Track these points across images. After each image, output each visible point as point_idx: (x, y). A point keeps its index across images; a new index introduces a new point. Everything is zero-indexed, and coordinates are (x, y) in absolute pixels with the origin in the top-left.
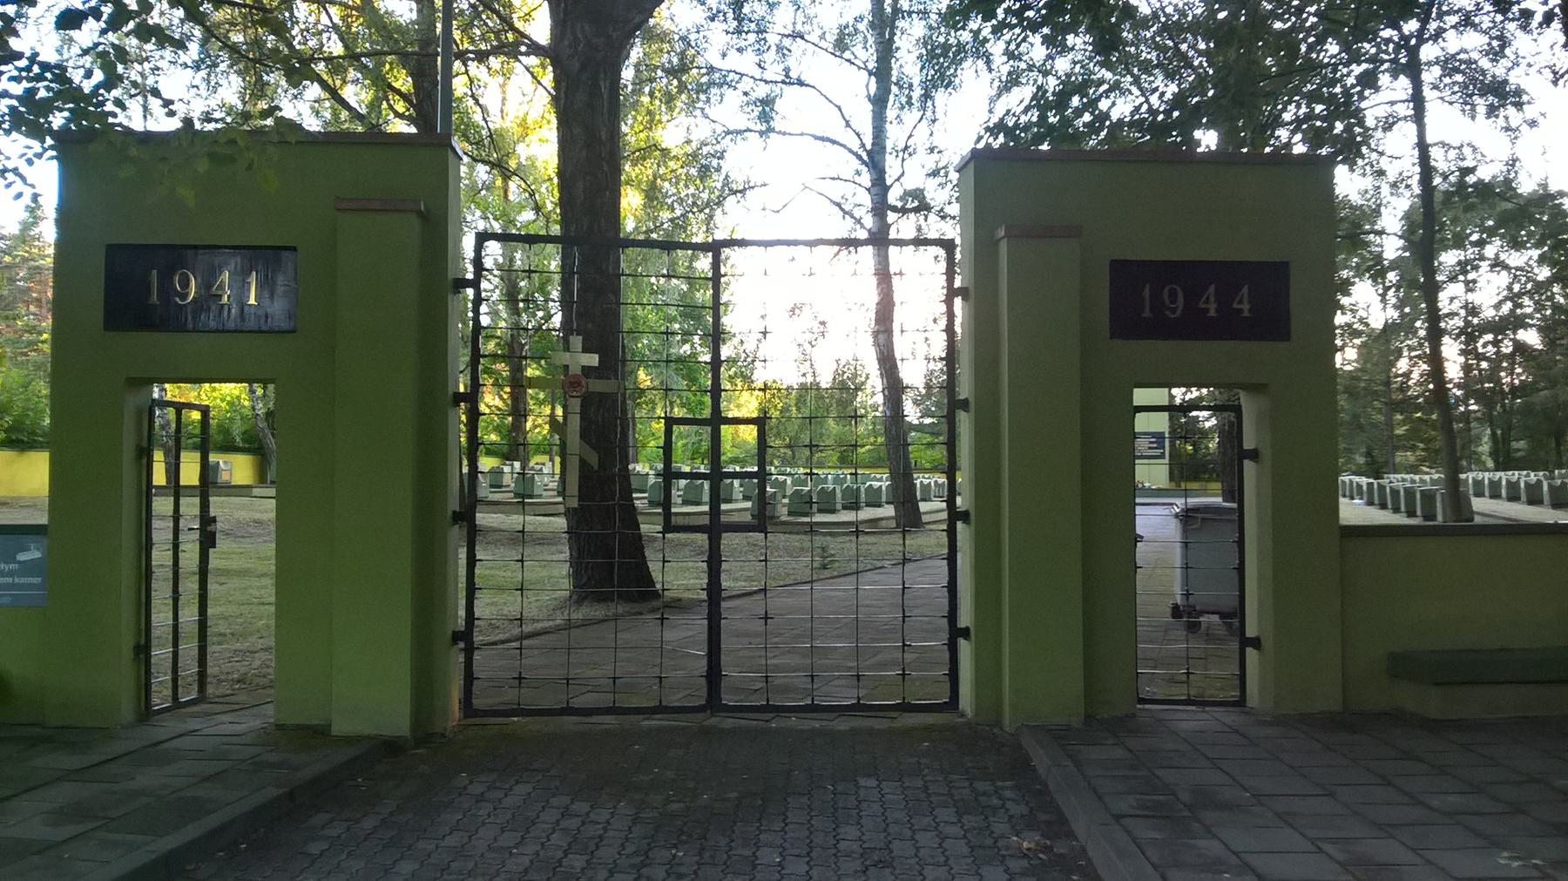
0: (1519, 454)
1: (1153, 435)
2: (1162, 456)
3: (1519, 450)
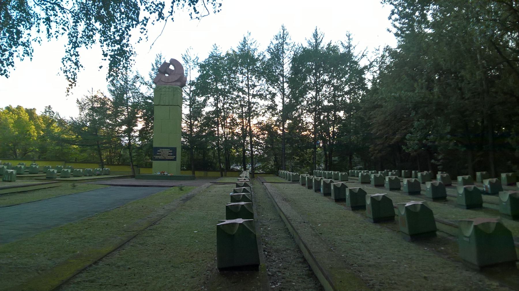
0: (335, 162)
1: (171, 149)
2: (175, 159)
3: (335, 161)
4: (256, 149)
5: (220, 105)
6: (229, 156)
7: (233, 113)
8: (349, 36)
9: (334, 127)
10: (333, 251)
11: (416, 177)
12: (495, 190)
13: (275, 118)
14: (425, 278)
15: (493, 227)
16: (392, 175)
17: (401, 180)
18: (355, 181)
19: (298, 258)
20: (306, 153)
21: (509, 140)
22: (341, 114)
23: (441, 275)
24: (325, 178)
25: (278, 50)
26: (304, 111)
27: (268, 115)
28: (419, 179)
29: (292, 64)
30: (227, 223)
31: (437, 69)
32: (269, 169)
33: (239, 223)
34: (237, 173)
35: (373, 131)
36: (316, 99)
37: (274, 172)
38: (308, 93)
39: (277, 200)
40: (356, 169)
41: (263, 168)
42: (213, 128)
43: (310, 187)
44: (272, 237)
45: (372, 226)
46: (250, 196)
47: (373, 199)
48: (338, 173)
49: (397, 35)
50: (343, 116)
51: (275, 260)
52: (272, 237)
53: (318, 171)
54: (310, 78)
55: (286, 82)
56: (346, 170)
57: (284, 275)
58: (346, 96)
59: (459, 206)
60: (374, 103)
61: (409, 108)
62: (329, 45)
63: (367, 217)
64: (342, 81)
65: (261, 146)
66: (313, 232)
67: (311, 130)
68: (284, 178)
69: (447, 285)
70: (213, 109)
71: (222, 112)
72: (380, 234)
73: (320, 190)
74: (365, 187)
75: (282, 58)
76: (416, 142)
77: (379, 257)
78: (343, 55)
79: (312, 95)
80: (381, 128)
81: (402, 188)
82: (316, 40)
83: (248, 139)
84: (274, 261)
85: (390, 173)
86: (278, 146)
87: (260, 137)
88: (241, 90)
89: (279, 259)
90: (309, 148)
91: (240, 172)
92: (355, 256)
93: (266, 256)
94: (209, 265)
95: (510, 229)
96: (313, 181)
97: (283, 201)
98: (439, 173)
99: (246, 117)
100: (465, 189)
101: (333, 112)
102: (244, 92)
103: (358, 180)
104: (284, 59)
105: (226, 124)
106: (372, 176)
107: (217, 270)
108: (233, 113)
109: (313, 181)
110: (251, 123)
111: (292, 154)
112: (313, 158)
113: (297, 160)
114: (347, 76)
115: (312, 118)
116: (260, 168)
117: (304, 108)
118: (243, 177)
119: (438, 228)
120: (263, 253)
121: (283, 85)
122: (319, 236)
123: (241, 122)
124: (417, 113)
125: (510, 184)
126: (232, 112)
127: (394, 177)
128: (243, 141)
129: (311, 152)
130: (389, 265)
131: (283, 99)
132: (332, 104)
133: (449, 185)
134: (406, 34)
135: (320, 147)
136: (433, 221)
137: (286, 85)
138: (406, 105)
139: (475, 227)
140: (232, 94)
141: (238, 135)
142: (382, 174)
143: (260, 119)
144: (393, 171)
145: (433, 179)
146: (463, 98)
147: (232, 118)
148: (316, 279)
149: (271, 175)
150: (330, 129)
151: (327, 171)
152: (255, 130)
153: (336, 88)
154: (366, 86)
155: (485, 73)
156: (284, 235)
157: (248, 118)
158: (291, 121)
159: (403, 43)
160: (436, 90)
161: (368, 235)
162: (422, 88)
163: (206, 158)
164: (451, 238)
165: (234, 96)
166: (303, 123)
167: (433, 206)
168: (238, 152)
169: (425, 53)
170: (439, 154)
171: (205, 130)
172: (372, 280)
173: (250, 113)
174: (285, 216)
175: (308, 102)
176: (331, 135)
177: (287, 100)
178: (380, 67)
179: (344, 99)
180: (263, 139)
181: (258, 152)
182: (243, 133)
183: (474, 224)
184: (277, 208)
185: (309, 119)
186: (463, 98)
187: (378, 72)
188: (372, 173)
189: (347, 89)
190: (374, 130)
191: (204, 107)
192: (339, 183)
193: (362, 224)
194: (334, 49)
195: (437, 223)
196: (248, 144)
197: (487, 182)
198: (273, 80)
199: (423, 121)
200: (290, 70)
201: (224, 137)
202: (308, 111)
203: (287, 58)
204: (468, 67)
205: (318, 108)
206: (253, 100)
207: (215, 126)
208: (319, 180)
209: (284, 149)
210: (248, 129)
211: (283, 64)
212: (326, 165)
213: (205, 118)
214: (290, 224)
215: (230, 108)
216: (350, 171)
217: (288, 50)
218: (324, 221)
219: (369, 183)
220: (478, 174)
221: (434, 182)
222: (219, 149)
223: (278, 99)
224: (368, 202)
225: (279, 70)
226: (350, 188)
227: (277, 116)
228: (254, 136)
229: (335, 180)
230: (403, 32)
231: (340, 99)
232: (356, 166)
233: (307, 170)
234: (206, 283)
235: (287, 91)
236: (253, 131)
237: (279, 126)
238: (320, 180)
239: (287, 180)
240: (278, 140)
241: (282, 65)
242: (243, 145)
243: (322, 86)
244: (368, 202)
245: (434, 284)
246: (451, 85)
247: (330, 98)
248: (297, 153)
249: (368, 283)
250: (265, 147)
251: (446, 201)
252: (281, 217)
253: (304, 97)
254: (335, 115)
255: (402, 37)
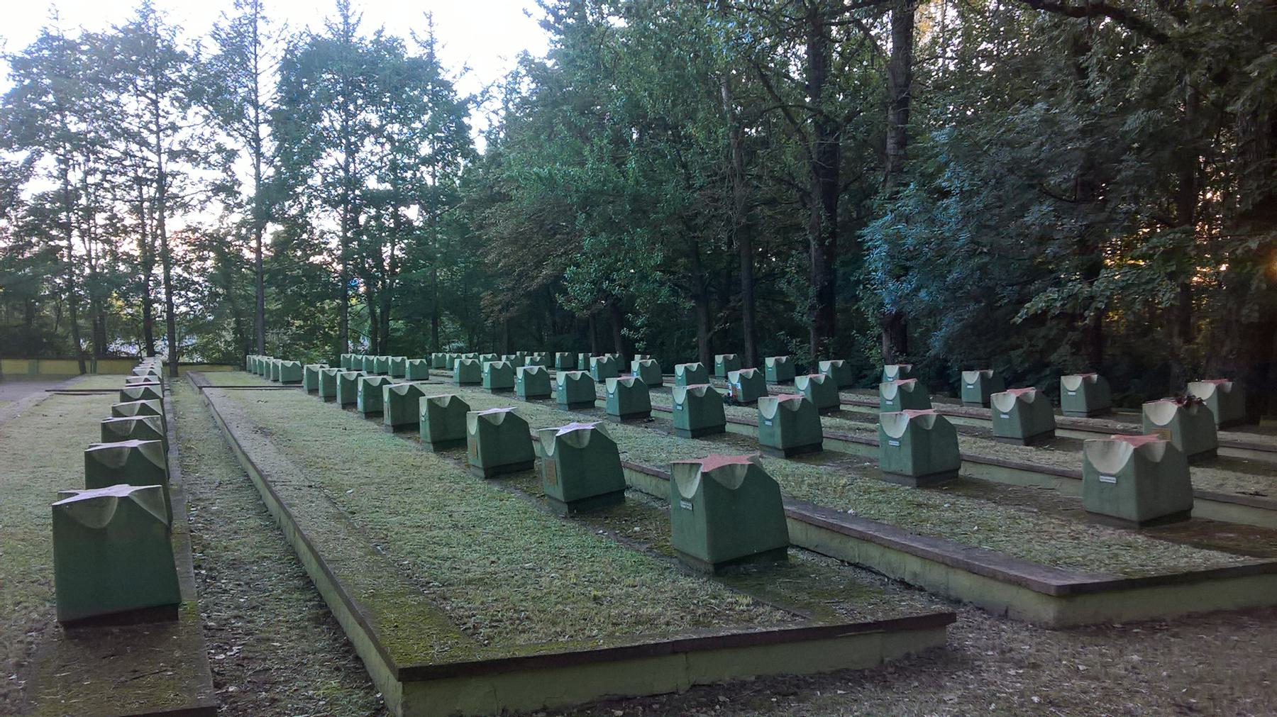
0: (398, 334)
3: (398, 330)
4: (181, 300)
5: (75, 177)
6: (102, 318)
7: (115, 199)
8: (431, 16)
9: (393, 245)
10: (381, 554)
11: (587, 368)
12: (752, 393)
13: (236, 217)
14: (596, 598)
15: (741, 474)
16: (533, 363)
17: (551, 376)
18: (446, 380)
19: (291, 577)
20: (323, 311)
21: (783, 285)
22: (413, 213)
23: (631, 589)
24: (370, 373)
25: (239, 34)
26: (315, 203)
27: (216, 207)
28: (593, 374)
29: (283, 75)
30: (83, 498)
31: (636, 114)
32: (219, 351)
33: (119, 498)
34: (128, 363)
35: (489, 258)
36: (346, 170)
37: (234, 360)
38: (324, 154)
39: (237, 433)
40: (450, 351)
41: (201, 349)
42: (53, 238)
43: (330, 398)
44: (223, 528)
45: (481, 485)
46: (159, 422)
47: (481, 419)
48: (403, 361)
49: (545, 25)
50: (418, 219)
51: (228, 588)
52: (223, 528)
53: (353, 355)
54: (330, 116)
55: (266, 121)
56: (424, 353)
57: (250, 625)
58: (423, 168)
59: (679, 432)
60: (492, 188)
61: (573, 205)
62: (379, 33)
63: (468, 466)
64: (413, 130)
65: (196, 291)
66: (331, 510)
67: (335, 252)
68: (262, 375)
69: (644, 611)
70: (55, 186)
71: (79, 197)
72: (498, 503)
73: (355, 404)
74: (467, 395)
75: (254, 56)
76: (587, 285)
77: (493, 558)
78: (416, 64)
79: (336, 160)
80: (508, 250)
81: (553, 395)
82: (346, 17)
83: (158, 270)
84: (225, 591)
85: (528, 359)
86: (245, 291)
87: (194, 267)
88: (129, 135)
89: (239, 585)
90: (329, 299)
91: (136, 360)
92: (436, 561)
93: (205, 581)
94: (35, 616)
95: (779, 480)
96: (338, 382)
97: (254, 436)
98: (637, 357)
99: (152, 211)
100: (690, 393)
101: (391, 209)
102: (144, 143)
103: (452, 377)
104: (258, 58)
105: (93, 229)
106: (486, 367)
107: (57, 627)
108: (115, 199)
109: (338, 382)
110: (167, 228)
111: (281, 313)
112: (339, 324)
113: (297, 327)
114: (426, 118)
115: (337, 219)
116: (195, 350)
117: (315, 194)
118: (143, 373)
119: (628, 483)
120: (193, 571)
121: (257, 129)
122: (346, 518)
123: (137, 226)
124: (589, 216)
125: (781, 382)
126: (109, 196)
127: (536, 369)
128: (143, 277)
129: (335, 309)
130: (515, 577)
131: (257, 168)
132: (388, 186)
133: (658, 386)
134: (567, 26)
135: (358, 296)
136: (618, 467)
137: (265, 130)
138: (566, 196)
139: (704, 474)
140: (110, 147)
141: (129, 259)
142: (508, 363)
143: (193, 218)
144: (536, 354)
145: (623, 371)
146: (690, 187)
147: (109, 213)
148: (336, 626)
149: (225, 367)
150: (384, 249)
151: (375, 355)
152: (179, 250)
153: (402, 147)
154: (471, 146)
155: (738, 132)
156: (257, 522)
157: (156, 215)
158: (280, 228)
159: (559, 46)
160: (632, 164)
161: (469, 509)
162: (601, 160)
163: (35, 324)
164: (656, 504)
165: (116, 154)
166: (312, 233)
167: (619, 433)
168: (131, 305)
169: (609, 75)
170: (637, 314)
171: (30, 245)
172: (474, 615)
173: (164, 202)
174: (259, 472)
175: (324, 177)
176: (385, 264)
177: (268, 171)
178: (506, 102)
179: (418, 175)
180: (202, 272)
181: (188, 305)
182: (144, 252)
183: (702, 469)
184: (239, 453)
185: (327, 222)
186: (690, 187)
187: (503, 113)
188: (486, 360)
189: (425, 149)
190: (493, 255)
191: (27, 180)
192: (403, 385)
193: (458, 483)
194: (392, 47)
195: (626, 473)
196: (158, 284)
197: (734, 377)
198: (229, 114)
199: (603, 236)
200: (275, 90)
201: (87, 264)
202: (325, 201)
203: (267, 58)
204: (701, 115)
205: (352, 196)
206: (169, 167)
207: (62, 235)
208: (353, 378)
209: (261, 298)
210: (158, 243)
211: (257, 74)
212: (373, 341)
213: (32, 211)
214: (272, 493)
215: (106, 185)
216: (433, 355)
217: (269, 38)
218: (363, 481)
219: (478, 383)
220: (719, 359)
221: (624, 378)
222: (74, 300)
223: (243, 167)
224: (473, 428)
225: (246, 89)
226: (431, 397)
227: (240, 210)
228: (175, 264)
229: (395, 377)
230: (559, 19)
231: (409, 174)
232: (449, 343)
233: (325, 355)
234: (22, 666)
235: (269, 147)
236: (172, 250)
237: (246, 239)
238: (357, 377)
239: (269, 381)
240: (244, 276)
241: (254, 76)
242: (143, 288)
243: (362, 138)
244: (473, 428)
245: (614, 612)
246: (664, 156)
247: (383, 170)
248: (298, 309)
249: (465, 624)
250: (206, 293)
251: (650, 421)
252: (248, 476)
253: (315, 164)
254: (395, 216)
255: (558, 32)
